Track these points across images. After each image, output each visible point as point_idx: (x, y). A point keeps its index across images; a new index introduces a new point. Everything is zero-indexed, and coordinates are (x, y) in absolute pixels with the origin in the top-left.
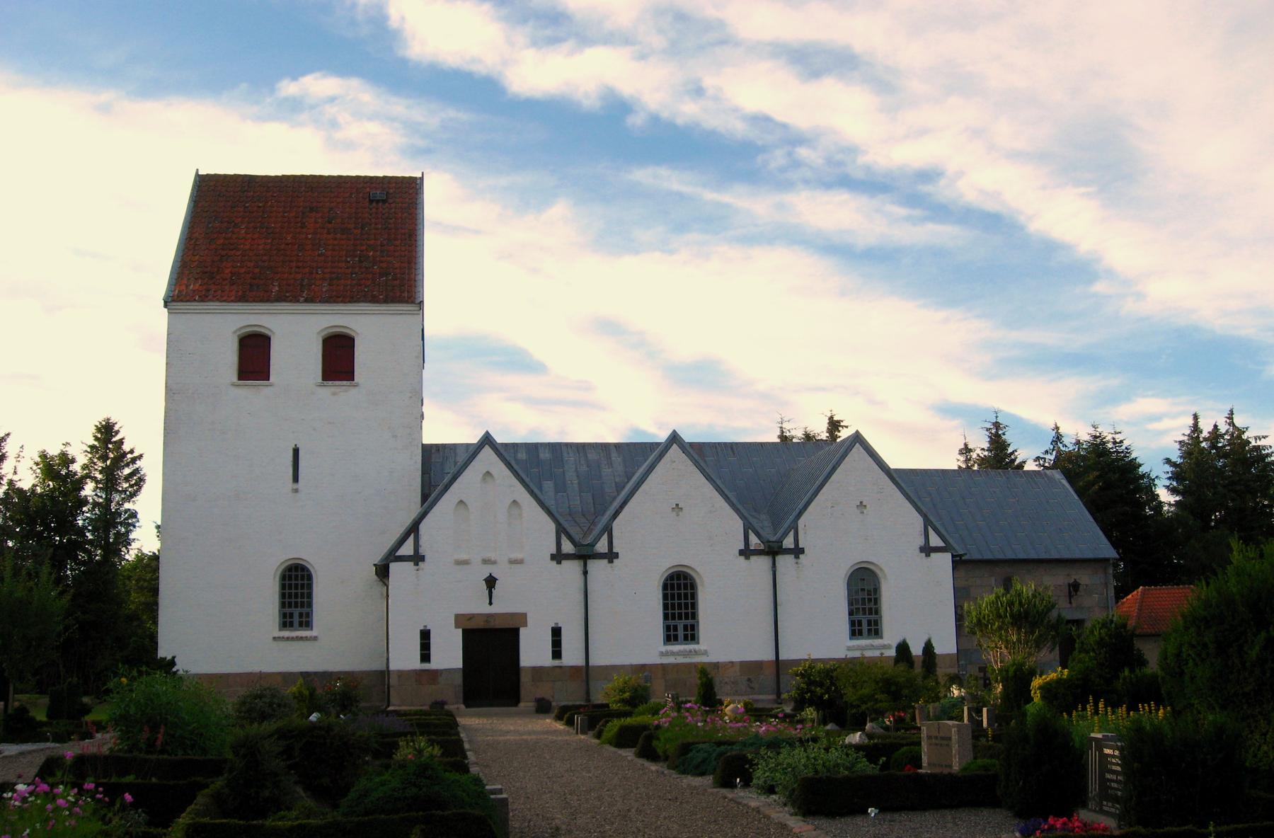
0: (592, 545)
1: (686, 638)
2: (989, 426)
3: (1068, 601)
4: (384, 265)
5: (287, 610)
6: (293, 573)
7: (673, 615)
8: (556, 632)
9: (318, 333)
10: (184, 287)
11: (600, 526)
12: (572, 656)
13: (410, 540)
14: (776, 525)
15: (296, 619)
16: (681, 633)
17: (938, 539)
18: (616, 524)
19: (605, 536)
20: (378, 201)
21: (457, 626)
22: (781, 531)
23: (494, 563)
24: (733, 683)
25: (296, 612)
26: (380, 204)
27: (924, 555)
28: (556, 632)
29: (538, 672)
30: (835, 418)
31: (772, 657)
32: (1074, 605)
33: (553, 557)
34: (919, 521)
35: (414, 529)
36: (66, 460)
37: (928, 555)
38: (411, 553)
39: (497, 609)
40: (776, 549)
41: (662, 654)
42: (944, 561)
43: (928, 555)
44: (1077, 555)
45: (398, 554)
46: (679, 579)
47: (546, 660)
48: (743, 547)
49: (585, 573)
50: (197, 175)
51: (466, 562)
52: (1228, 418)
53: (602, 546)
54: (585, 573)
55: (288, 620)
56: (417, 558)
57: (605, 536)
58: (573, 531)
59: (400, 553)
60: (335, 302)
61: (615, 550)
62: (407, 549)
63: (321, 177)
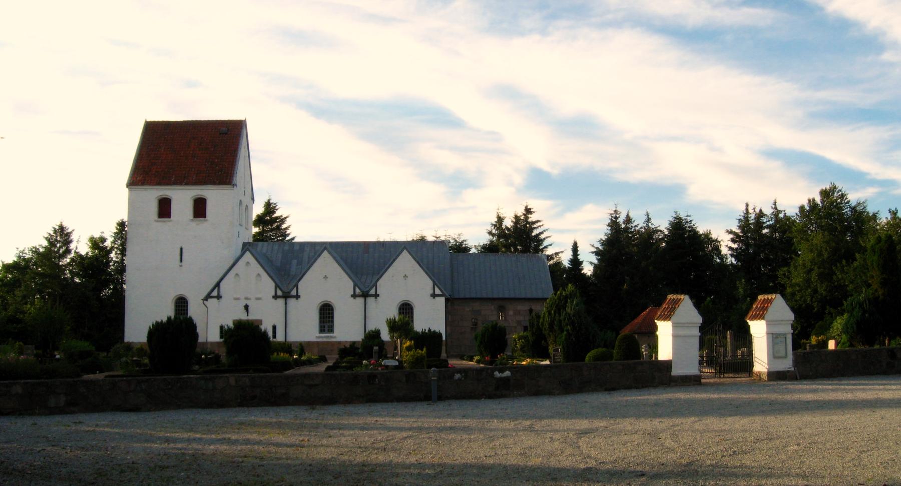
2: (613, 212)
4: (221, 166)
7: (324, 321)
9: (156, 198)
10: (135, 179)
11: (294, 284)
16: (326, 329)
17: (439, 291)
19: (295, 288)
20: (223, 133)
23: (249, 299)
27: (432, 297)
30: (529, 207)
33: (274, 297)
35: (218, 285)
36: (103, 240)
37: (434, 298)
38: (374, 293)
41: (317, 337)
42: (441, 301)
43: (434, 298)
45: (211, 295)
52: (774, 204)
53: (294, 293)
54: (286, 304)
56: (219, 297)
57: (295, 288)
61: (378, 293)
62: (215, 293)
63: (200, 121)
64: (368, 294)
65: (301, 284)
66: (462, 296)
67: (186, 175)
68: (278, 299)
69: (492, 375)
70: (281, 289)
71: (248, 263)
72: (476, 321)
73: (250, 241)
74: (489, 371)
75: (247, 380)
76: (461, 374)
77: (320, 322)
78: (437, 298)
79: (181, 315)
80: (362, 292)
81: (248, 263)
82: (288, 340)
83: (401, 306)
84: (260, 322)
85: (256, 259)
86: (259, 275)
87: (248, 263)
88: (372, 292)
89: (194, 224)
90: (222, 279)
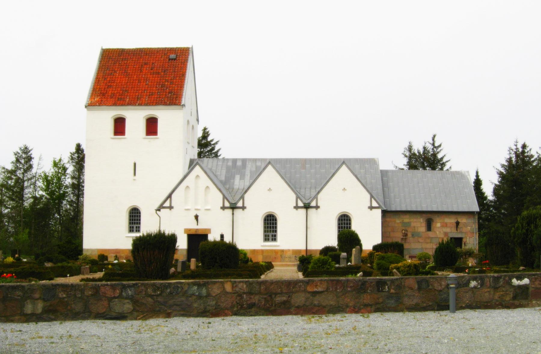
0: (236, 204)
3: (456, 229)
5: (132, 225)
6: (269, 218)
11: (240, 196)
13: (169, 200)
15: (135, 229)
20: (172, 59)
24: (289, 257)
25: (135, 226)
26: (173, 61)
31: (304, 248)
32: (458, 231)
34: (368, 196)
35: (170, 196)
41: (262, 246)
44: (461, 210)
49: (233, 214)
50: (102, 49)
51: (209, 210)
54: (233, 214)
56: (171, 207)
57: (315, 200)
59: (164, 205)
60: (150, 105)
61: (318, 205)
62: (167, 204)
64: (309, 206)
66: (393, 209)
67: (139, 96)
69: (509, 283)
72: (406, 233)
73: (195, 158)
74: (507, 278)
75: (245, 286)
76: (477, 281)
77: (265, 231)
78: (374, 210)
79: (135, 224)
82: (308, 248)
83: (266, 217)
84: (209, 231)
85: (206, 173)
86: (207, 187)
90: (173, 191)
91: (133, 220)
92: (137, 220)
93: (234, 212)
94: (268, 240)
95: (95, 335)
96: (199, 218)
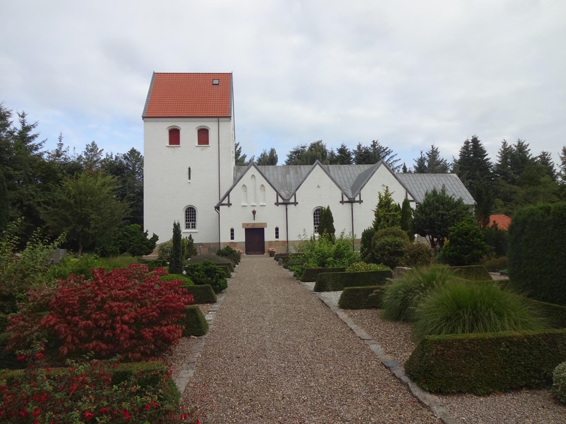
1: (192, 227)
5: (188, 223)
8: (277, 229)
9: (196, 128)
12: (282, 238)
14: (353, 192)
15: (191, 226)
16: (191, 226)
18: (297, 192)
21: (243, 228)
22: (355, 194)
25: (191, 223)
27: (276, 206)
28: (277, 229)
29: (271, 243)
33: (276, 204)
38: (227, 203)
39: (256, 221)
40: (353, 201)
43: (343, 204)
46: (191, 209)
47: (273, 239)
48: (276, 202)
49: (287, 209)
54: (287, 209)
55: (193, 226)
56: (229, 204)
58: (283, 194)
59: (223, 203)
61: (230, 203)
65: (362, 192)
68: (279, 205)
70: (347, 196)
71: (253, 176)
80: (349, 199)
81: (253, 176)
87: (253, 175)
88: (292, 200)
89: (199, 149)
91: (188, 218)
92: (193, 218)
93: (288, 208)
94: (189, 227)
95: (416, 397)
96: (256, 213)
